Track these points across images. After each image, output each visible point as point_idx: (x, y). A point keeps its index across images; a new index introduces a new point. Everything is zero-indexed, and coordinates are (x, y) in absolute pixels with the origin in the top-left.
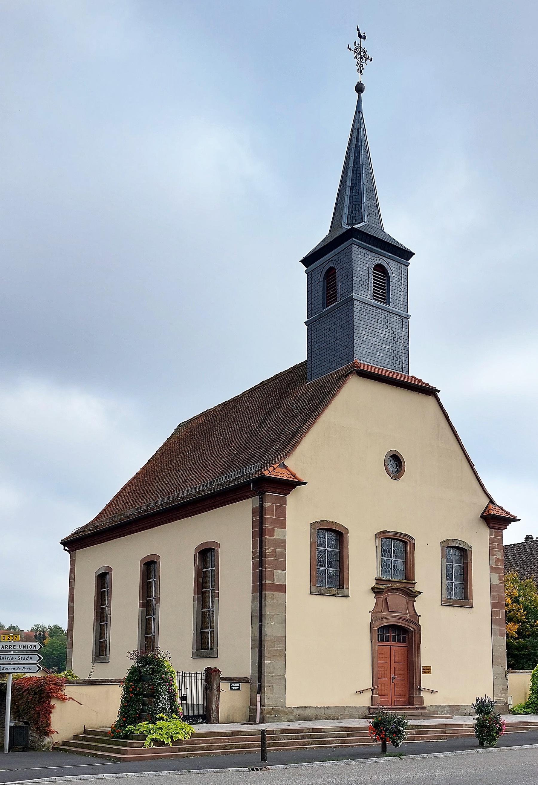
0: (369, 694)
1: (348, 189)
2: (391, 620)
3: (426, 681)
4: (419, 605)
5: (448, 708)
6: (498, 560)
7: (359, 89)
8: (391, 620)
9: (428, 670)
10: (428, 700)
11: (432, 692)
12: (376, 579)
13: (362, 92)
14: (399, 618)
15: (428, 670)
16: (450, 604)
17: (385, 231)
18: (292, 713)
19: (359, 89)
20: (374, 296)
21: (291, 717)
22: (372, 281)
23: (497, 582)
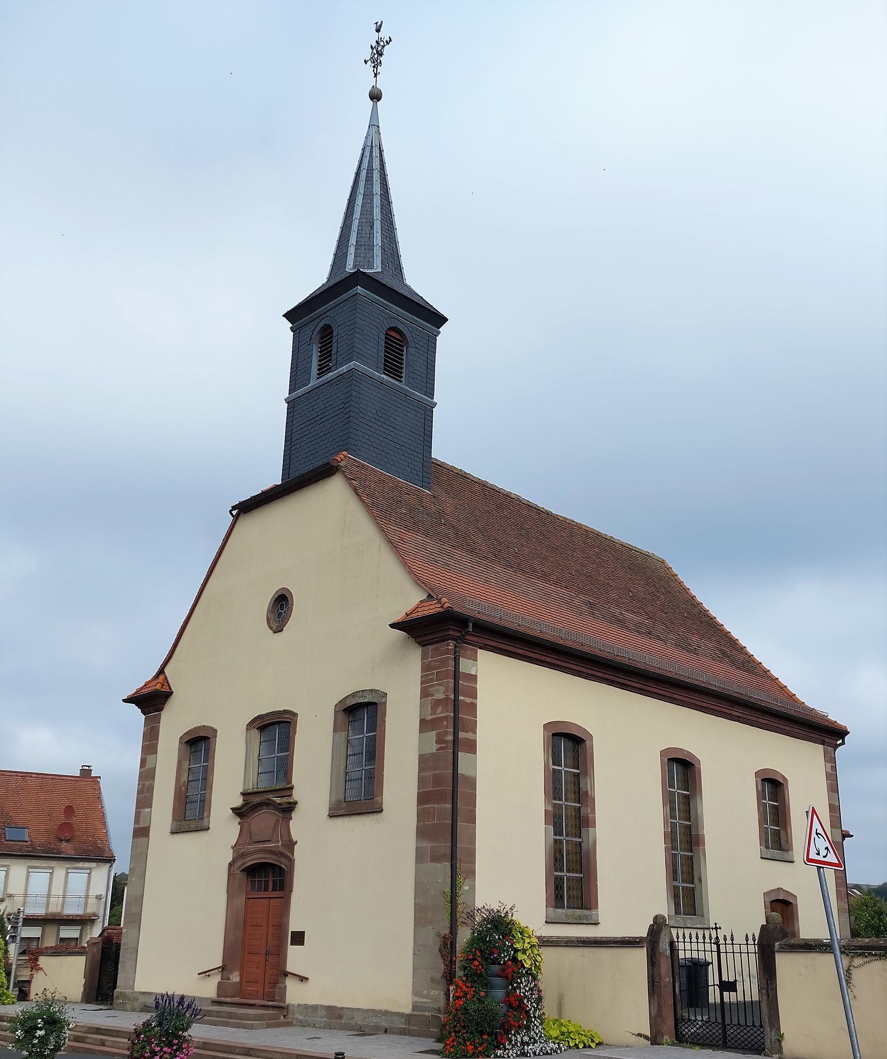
0: (216, 979)
1: (352, 250)
2: (256, 856)
3: (296, 958)
4: (298, 826)
5: (323, 1013)
6: (437, 703)
7: (375, 96)
8: (256, 856)
9: (299, 938)
10: (295, 994)
11: (303, 979)
12: (243, 794)
13: (379, 100)
14: (265, 851)
15: (299, 938)
16: (342, 812)
17: (325, 280)
18: (137, 1000)
19: (375, 96)
20: (385, 369)
21: (136, 1005)
22: (383, 349)
23: (433, 747)
